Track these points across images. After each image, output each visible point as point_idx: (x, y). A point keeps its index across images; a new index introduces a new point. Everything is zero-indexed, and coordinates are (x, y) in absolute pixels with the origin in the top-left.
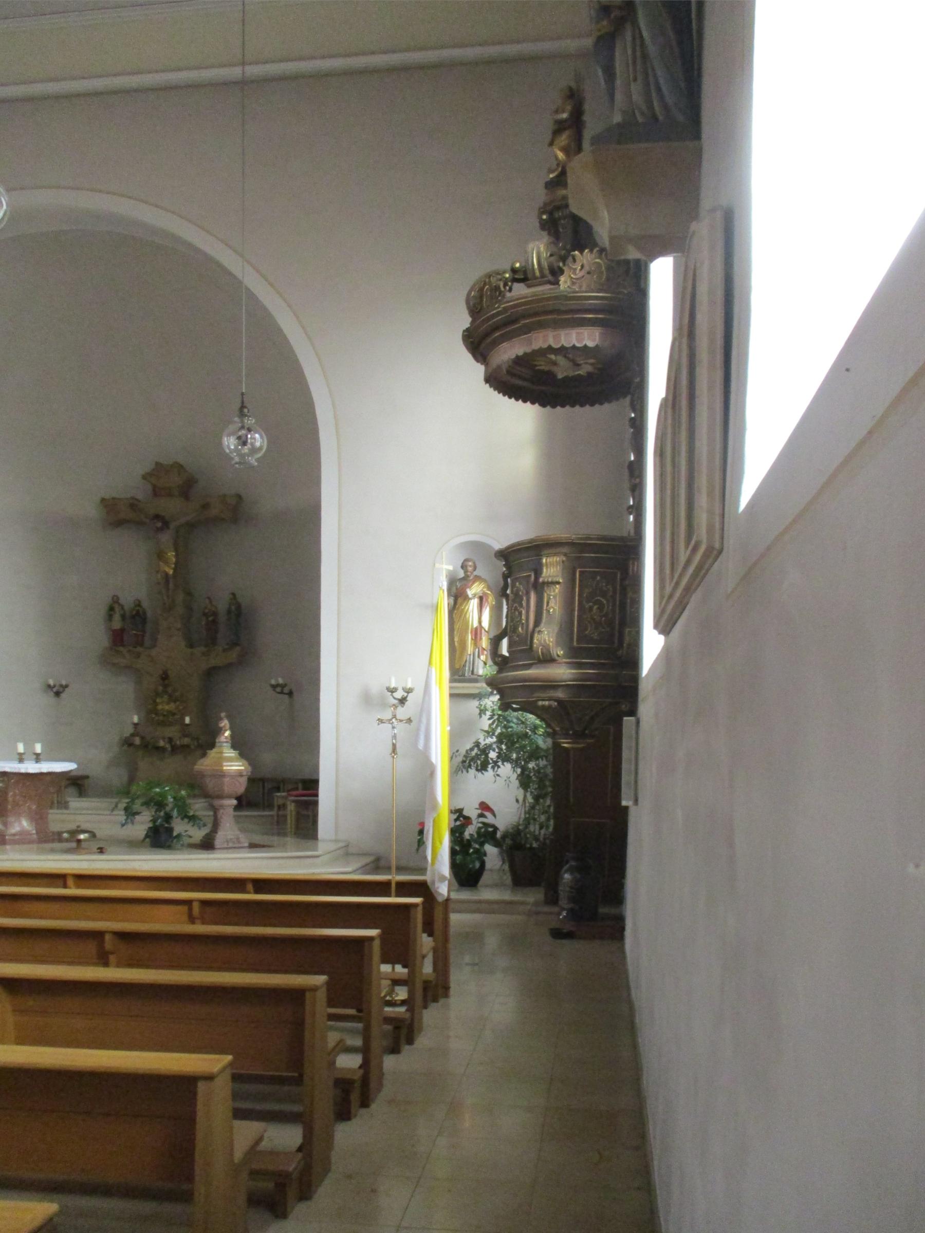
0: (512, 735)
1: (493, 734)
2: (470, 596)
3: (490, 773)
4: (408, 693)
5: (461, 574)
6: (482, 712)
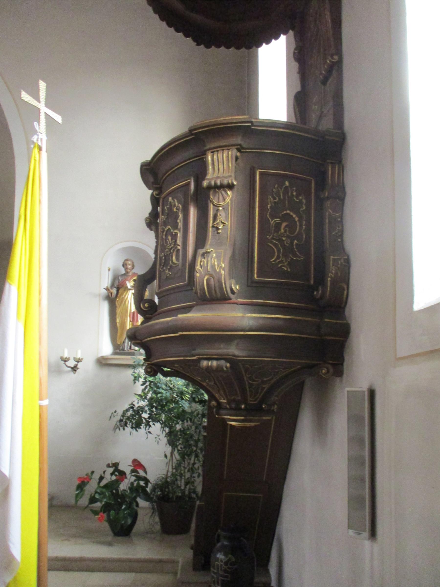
0: (161, 400)
1: (146, 398)
2: (129, 287)
3: (142, 430)
4: (78, 362)
5: (123, 271)
6: (136, 379)
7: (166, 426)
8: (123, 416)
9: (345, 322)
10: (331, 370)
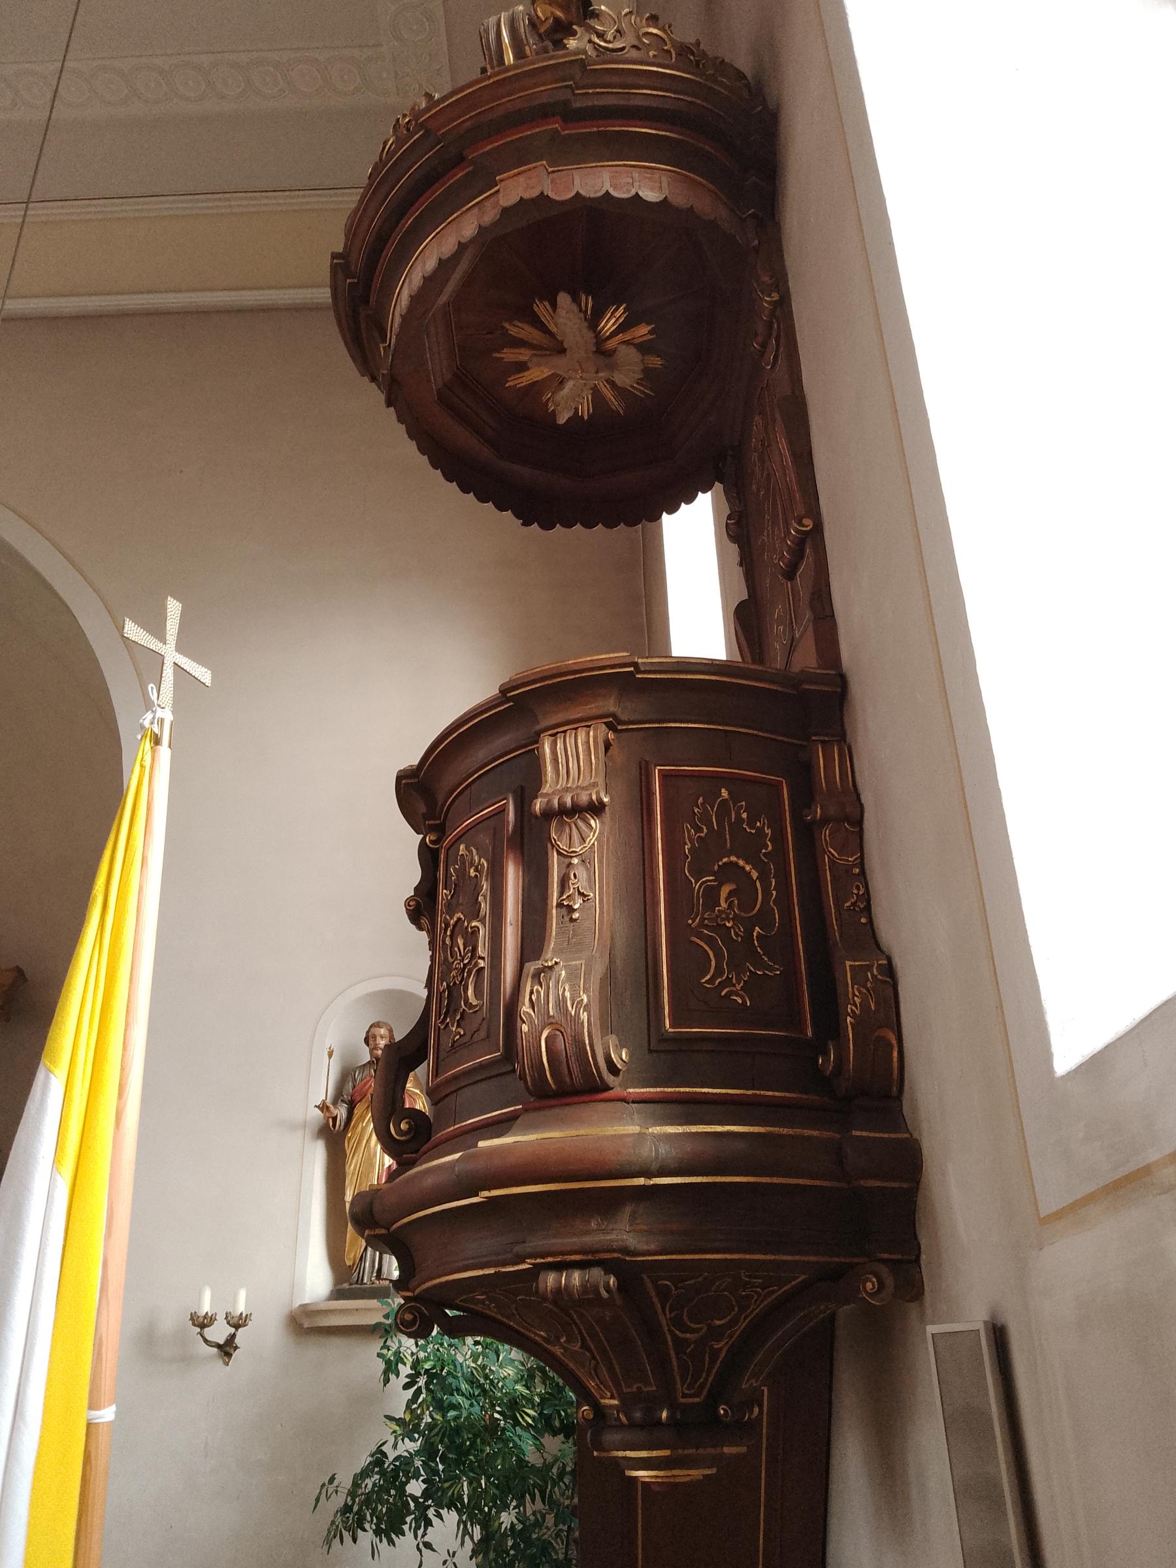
0: (457, 1431)
1: (416, 1428)
3: (407, 1542)
4: (237, 1327)
6: (391, 1368)
7: (472, 1519)
8: (352, 1494)
9: (906, 1135)
10: (890, 1282)
